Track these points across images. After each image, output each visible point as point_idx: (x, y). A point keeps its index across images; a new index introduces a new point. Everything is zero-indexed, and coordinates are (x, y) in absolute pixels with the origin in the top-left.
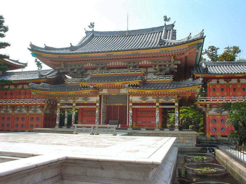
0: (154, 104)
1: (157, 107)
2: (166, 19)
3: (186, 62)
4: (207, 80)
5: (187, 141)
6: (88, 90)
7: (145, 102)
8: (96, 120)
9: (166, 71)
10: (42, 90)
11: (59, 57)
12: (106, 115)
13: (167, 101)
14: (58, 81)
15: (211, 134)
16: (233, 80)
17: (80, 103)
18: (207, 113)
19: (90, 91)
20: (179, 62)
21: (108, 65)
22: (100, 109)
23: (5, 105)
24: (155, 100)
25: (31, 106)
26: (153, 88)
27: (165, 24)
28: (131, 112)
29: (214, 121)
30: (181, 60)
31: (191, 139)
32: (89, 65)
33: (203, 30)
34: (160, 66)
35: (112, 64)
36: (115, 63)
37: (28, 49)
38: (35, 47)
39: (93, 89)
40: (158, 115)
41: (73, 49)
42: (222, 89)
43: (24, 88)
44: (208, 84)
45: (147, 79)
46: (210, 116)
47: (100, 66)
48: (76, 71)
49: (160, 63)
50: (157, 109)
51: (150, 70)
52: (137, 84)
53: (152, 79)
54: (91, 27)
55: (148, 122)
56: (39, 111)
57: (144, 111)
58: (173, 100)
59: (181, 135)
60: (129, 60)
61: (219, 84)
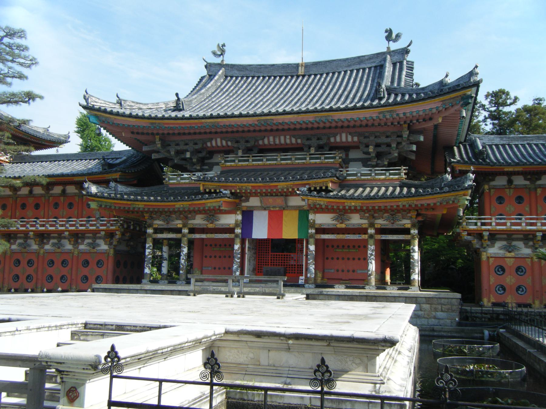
1: (371, 236)
2: (389, 36)
5: (440, 314)
7: (343, 226)
11: (152, 123)
15: (493, 300)
18: (484, 252)
21: (261, 142)
24: (365, 221)
27: (388, 48)
29: (500, 270)
32: (218, 142)
35: (269, 141)
46: (491, 259)
49: (379, 141)
51: (353, 155)
55: (348, 271)
56: (103, 247)
58: (406, 223)
61: (512, 186)
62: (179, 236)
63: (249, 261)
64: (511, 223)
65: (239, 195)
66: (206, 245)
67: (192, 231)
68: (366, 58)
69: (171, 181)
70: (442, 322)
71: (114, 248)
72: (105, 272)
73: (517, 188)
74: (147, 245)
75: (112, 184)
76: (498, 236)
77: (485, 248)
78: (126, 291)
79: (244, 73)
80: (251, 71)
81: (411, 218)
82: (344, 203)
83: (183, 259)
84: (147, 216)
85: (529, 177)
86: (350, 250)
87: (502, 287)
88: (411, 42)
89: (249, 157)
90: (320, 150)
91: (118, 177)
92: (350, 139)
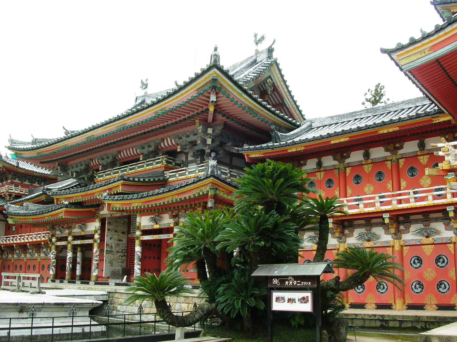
22: (101, 246)
29: (416, 261)
45: (170, 177)
46: (405, 248)
61: (322, 169)
73: (328, 171)
88: (274, 41)
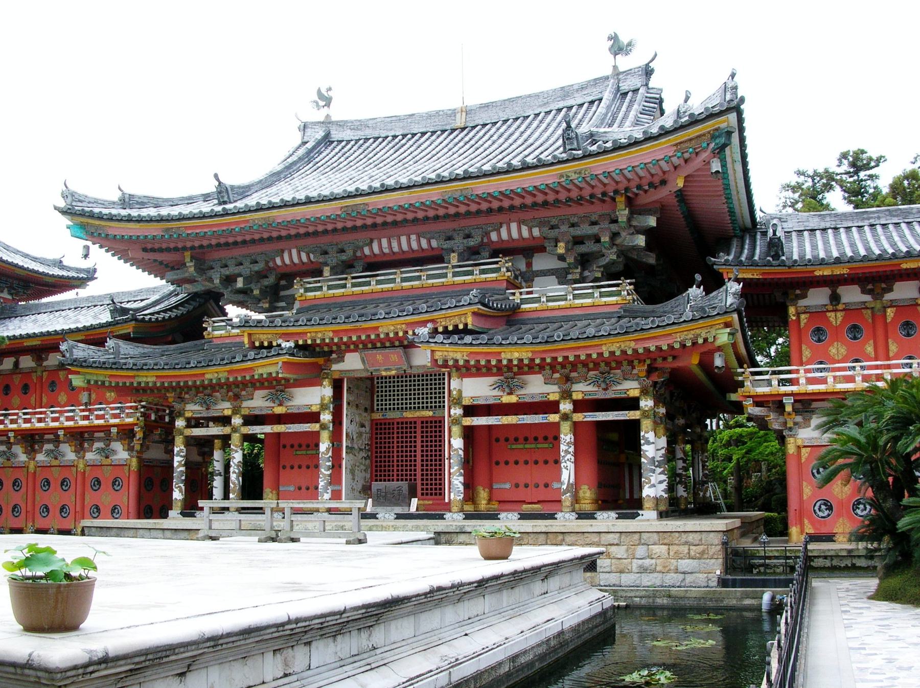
0: (553, 407)
1: (565, 417)
2: (618, 48)
3: (690, 215)
4: (786, 294)
5: (685, 564)
6: (275, 359)
7: (513, 399)
8: (321, 484)
9: (603, 261)
10: (106, 368)
11: (167, 230)
12: (368, 462)
13: (605, 389)
14: (182, 326)
15: (809, 529)
16: (898, 286)
17: (257, 412)
18: (791, 436)
19: (280, 364)
20: (652, 222)
21: (367, 251)
22: (336, 437)
23: (99, 428)
24: (555, 388)
25: (42, 438)
26: (528, 338)
27: (615, 67)
28: (458, 443)
30: (662, 210)
31: (703, 553)
32: (293, 257)
33: (733, 76)
34: (578, 241)
35: (381, 246)
36: (395, 245)
37: (56, 208)
38: (80, 201)
39: (292, 355)
40: (567, 452)
41: (226, 199)
42: (855, 329)
43: (21, 366)
44: (792, 310)
45: (524, 301)
46: (803, 450)
47: (334, 258)
48: (240, 283)
49: (578, 232)
50: (565, 427)
51: (540, 263)
52: (466, 325)
53: (544, 299)
54: (322, 103)
55: (537, 486)
56: (121, 453)
57: (304, 447)
58: (631, 388)
59: (655, 536)
60: (449, 225)
61: (840, 307)
62: (227, 430)
63: (352, 472)
64: (835, 377)
65: (318, 349)
66: (497, 440)
67: (251, 420)
68: (576, 87)
69: (216, 333)
70: (689, 579)
71: (137, 457)
72: (125, 499)
73: (849, 310)
74: (176, 450)
75: (110, 343)
76: (815, 405)
77: (790, 429)
78: (132, 532)
79: (362, 133)
80: (374, 128)
81: (637, 378)
82: (500, 353)
83: (234, 472)
84: (171, 395)
85: (870, 286)
86: (539, 446)
87: (825, 504)
89: (346, 279)
90: (474, 257)
91: (130, 330)
92: (525, 234)
